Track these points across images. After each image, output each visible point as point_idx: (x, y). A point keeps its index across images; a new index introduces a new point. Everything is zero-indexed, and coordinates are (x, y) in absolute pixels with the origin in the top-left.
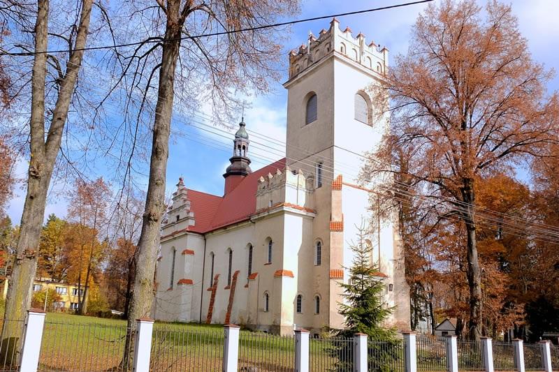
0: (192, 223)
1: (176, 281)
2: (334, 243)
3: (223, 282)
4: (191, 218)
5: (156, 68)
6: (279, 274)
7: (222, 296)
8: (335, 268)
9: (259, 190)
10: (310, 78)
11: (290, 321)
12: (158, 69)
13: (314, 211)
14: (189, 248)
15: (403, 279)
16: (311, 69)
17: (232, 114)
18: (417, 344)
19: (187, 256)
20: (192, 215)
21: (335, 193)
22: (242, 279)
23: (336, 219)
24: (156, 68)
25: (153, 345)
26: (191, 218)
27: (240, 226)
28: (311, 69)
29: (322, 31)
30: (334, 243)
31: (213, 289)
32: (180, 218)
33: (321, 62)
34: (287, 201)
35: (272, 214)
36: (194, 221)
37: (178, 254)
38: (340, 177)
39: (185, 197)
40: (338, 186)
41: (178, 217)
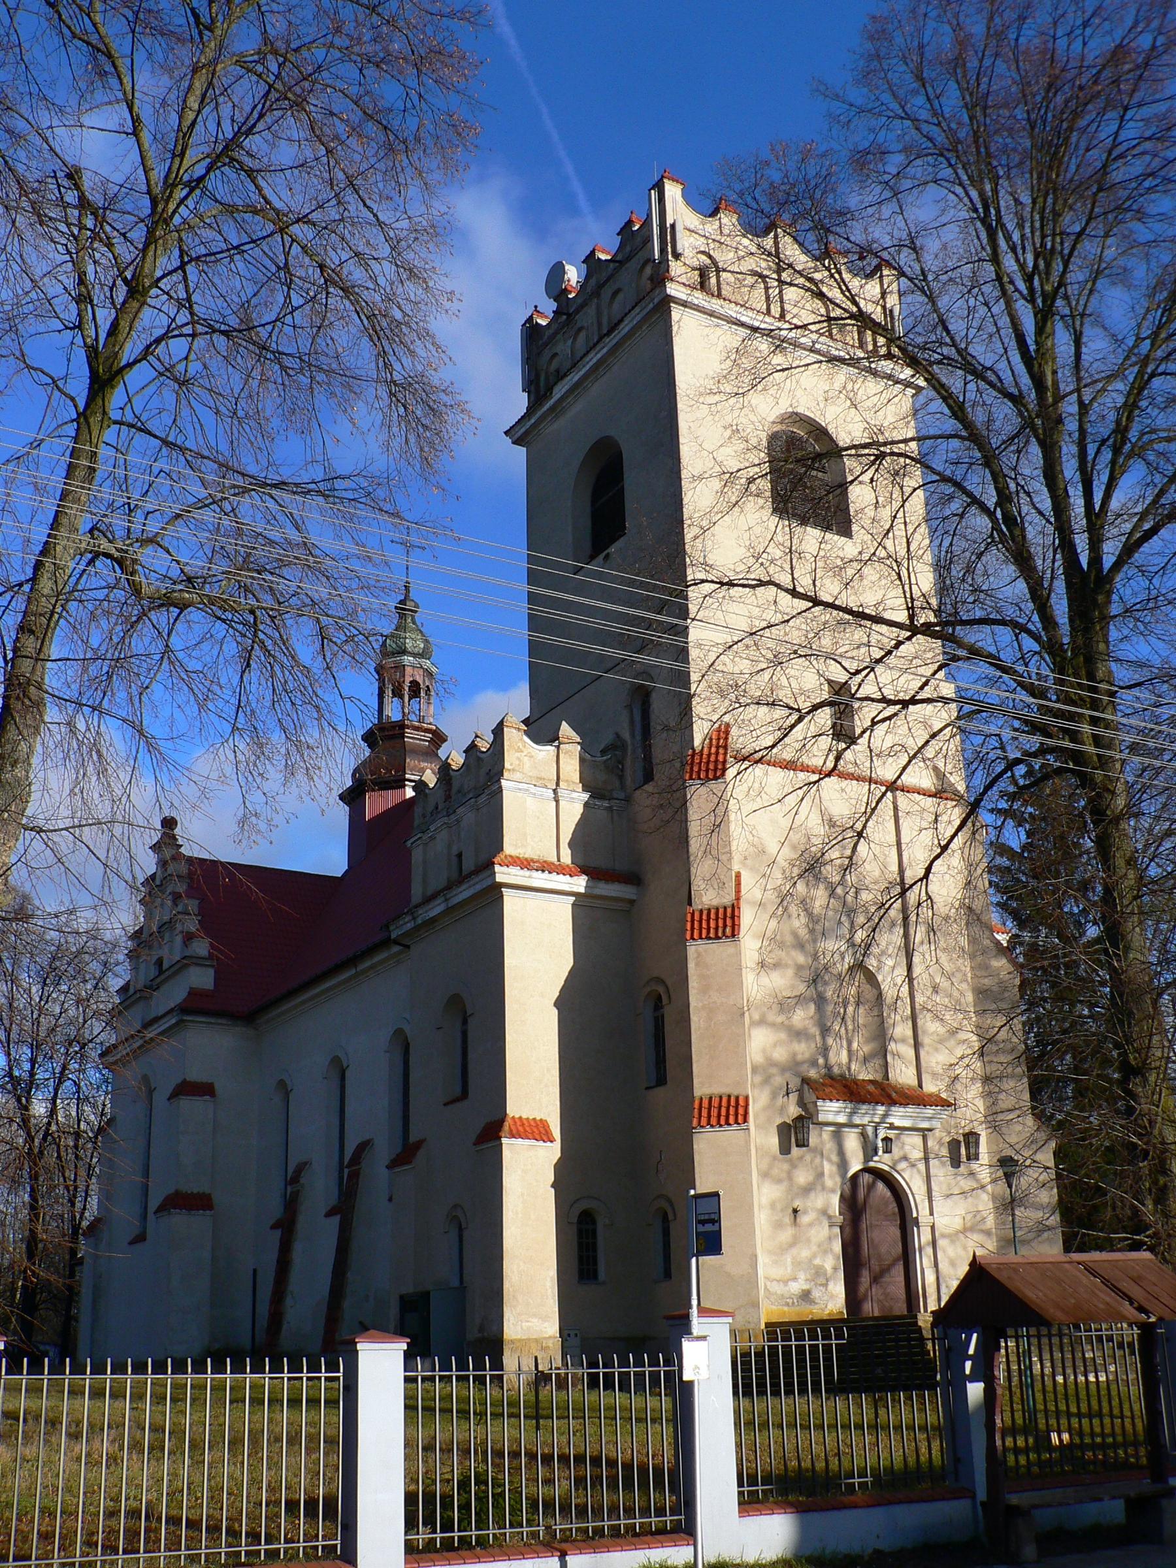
0: (202, 978)
1: (153, 1204)
2: (705, 990)
3: (321, 1189)
4: (197, 961)
5: (710, 257)
6: (492, 1129)
7: (317, 1240)
8: (717, 1089)
9: (416, 823)
10: (596, 389)
11: (544, 1319)
12: (708, 261)
13: (633, 878)
14: (195, 1074)
15: (1017, 1092)
16: (594, 358)
17: (1120, 385)
18: (407, 1380)
19: (186, 1104)
20: (201, 948)
21: (699, 798)
22: (377, 1171)
23: (707, 896)
24: (710, 257)
25: (739, 1445)
26: (197, 961)
27: (361, 967)
28: (594, 358)
29: (630, 223)
30: (705, 990)
31: (287, 1226)
32: (165, 965)
33: (625, 328)
34: (510, 846)
35: (461, 905)
36: (211, 972)
37: (160, 1097)
38: (722, 734)
39: (181, 888)
40: (713, 764)
41: (159, 962)
